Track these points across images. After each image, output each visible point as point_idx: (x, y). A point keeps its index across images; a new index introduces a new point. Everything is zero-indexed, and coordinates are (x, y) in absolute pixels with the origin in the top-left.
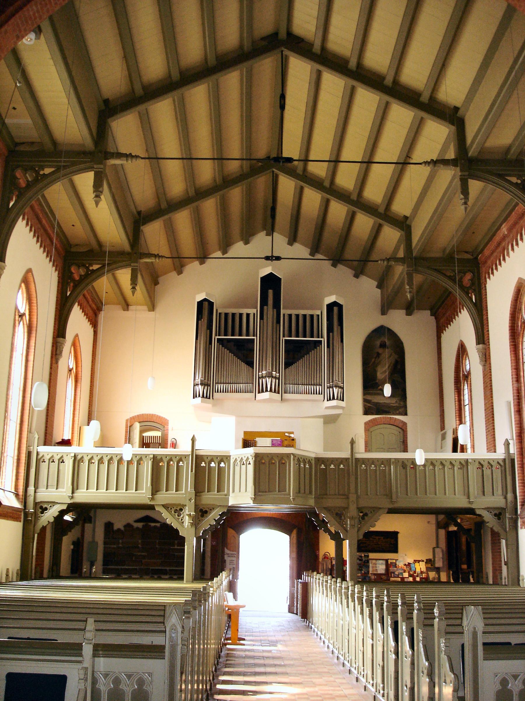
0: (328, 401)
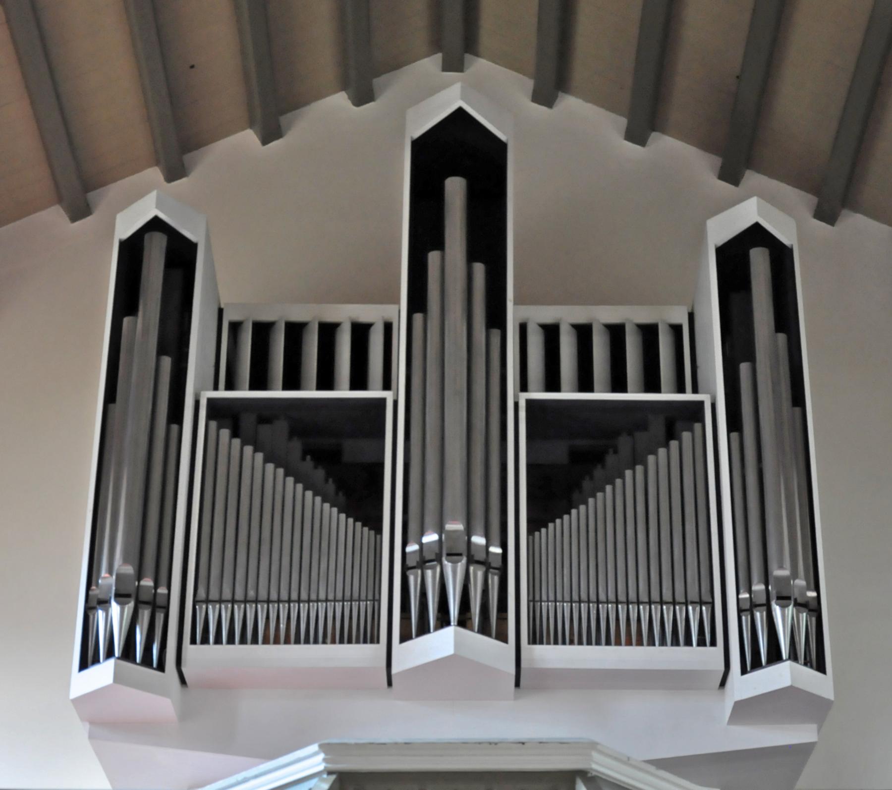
0: (744, 671)
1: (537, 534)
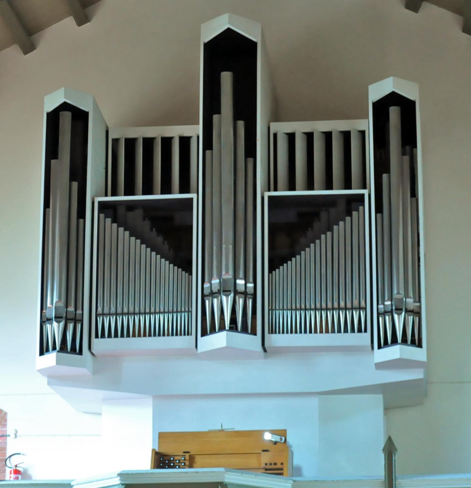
0: (380, 347)
1: (274, 272)
